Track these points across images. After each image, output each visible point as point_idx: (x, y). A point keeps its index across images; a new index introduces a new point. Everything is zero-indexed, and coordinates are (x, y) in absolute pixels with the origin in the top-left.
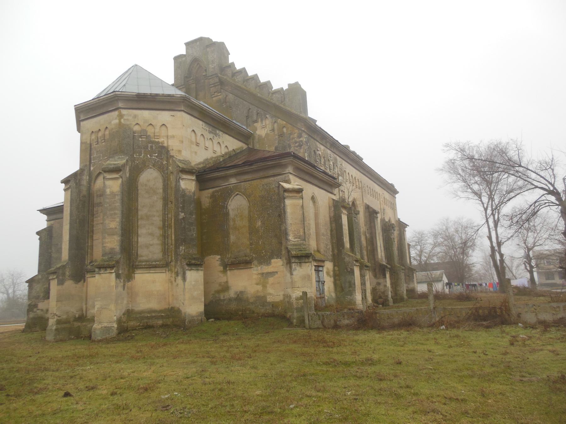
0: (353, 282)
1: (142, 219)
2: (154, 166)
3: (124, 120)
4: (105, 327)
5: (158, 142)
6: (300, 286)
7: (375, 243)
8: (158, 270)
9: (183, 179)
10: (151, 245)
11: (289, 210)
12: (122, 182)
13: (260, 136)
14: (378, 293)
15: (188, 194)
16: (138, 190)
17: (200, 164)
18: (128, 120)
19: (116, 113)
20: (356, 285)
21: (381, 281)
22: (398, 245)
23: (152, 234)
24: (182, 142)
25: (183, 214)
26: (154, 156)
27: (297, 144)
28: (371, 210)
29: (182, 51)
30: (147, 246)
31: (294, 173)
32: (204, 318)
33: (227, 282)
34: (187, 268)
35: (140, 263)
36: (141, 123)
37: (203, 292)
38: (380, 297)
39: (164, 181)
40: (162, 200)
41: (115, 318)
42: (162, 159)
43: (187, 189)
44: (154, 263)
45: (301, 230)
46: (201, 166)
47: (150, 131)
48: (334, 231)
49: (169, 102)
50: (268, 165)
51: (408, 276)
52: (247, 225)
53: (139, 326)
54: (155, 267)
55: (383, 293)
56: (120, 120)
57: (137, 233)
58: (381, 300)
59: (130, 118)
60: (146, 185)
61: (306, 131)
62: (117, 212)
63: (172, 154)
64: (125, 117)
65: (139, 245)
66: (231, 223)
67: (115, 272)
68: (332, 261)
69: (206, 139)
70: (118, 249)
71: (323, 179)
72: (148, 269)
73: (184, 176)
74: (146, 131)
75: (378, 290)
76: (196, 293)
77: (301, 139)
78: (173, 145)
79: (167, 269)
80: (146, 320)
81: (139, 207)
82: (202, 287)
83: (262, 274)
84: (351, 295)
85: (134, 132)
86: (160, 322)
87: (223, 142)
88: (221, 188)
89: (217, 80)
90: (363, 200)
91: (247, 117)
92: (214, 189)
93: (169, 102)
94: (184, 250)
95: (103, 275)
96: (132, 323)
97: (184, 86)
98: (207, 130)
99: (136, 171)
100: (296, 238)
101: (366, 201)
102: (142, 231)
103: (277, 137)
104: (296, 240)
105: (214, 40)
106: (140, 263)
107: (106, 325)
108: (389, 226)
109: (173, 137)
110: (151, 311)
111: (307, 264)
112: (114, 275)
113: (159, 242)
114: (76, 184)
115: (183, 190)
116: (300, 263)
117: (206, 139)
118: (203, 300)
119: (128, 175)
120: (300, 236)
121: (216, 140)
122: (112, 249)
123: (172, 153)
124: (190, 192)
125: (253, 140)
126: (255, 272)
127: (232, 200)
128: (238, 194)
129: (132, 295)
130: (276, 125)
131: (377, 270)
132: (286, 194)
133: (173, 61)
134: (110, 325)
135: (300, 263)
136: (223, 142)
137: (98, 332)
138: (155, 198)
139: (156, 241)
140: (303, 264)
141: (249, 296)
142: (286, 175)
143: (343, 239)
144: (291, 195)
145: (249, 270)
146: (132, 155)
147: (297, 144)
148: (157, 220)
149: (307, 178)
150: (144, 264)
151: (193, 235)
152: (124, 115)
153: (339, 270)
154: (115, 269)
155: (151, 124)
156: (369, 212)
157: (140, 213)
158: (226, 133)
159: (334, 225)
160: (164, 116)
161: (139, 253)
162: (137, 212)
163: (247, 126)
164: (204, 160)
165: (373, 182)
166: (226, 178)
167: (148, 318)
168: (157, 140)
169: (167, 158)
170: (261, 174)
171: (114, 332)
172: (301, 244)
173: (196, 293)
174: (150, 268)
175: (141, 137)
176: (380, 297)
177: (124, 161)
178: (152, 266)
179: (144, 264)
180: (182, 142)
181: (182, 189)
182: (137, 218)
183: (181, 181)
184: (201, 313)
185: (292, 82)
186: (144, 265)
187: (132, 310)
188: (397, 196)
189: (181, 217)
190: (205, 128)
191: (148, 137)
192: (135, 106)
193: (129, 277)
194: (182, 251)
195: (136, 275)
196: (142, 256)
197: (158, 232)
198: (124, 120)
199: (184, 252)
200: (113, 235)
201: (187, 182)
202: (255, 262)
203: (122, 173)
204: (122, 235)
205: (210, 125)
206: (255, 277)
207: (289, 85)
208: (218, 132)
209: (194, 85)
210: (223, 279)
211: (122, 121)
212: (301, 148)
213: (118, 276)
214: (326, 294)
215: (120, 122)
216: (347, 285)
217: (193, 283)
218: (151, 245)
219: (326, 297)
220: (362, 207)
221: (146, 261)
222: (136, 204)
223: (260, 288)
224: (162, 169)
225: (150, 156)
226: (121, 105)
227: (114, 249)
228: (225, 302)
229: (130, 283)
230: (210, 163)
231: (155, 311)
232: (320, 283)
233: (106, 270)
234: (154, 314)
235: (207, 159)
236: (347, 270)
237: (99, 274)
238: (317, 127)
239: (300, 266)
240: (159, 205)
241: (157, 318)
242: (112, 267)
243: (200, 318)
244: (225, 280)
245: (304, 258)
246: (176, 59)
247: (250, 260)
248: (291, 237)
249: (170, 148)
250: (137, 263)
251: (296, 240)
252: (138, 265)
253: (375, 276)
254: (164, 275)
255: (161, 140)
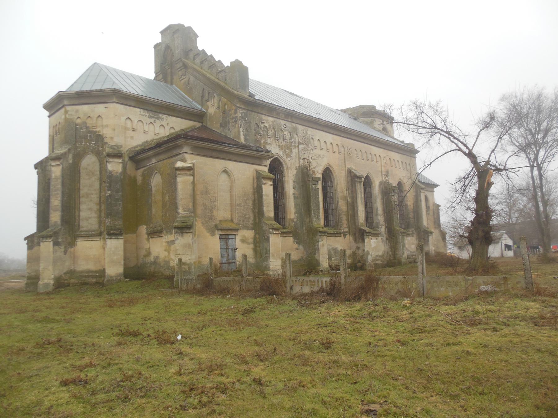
0: (268, 248)
1: (83, 196)
2: (92, 152)
3: (69, 115)
4: (46, 283)
5: (96, 132)
6: (181, 254)
7: (356, 208)
8: (94, 238)
9: (110, 162)
10: (90, 218)
11: (180, 186)
12: (63, 168)
13: (210, 114)
14: (358, 257)
15: (115, 174)
16: (80, 173)
17: (137, 146)
18: (71, 115)
19: (63, 110)
20: (271, 251)
21: (360, 245)
22: (414, 207)
23: (90, 209)
24: (114, 130)
25: (109, 192)
26: (93, 144)
27: (234, 120)
28: (352, 175)
29: (158, 39)
30: (87, 219)
31: (191, 152)
32: (122, 277)
33: (149, 248)
34: (107, 237)
35: (80, 233)
36: (81, 116)
37: (123, 257)
38: (359, 261)
39: (100, 164)
40: (98, 181)
41: (53, 277)
42: (98, 146)
43: (114, 171)
44: (91, 233)
45: (190, 203)
46: (139, 148)
47: (89, 122)
48: (257, 201)
49: (104, 96)
50: (170, 146)
51: (423, 239)
52: (161, 199)
53: (78, 283)
54: (92, 236)
55: (362, 257)
56: (65, 115)
57: (79, 209)
58: (360, 264)
59: (73, 113)
60: (86, 169)
61: (242, 106)
62: (58, 192)
63: (106, 141)
64: (69, 113)
65: (81, 218)
66: (153, 198)
67: (52, 241)
68: (252, 229)
69: (145, 124)
70: (59, 222)
71: (239, 153)
72: (87, 238)
73: (111, 160)
74: (86, 123)
75: (357, 255)
76: (115, 257)
77: (236, 115)
78: (107, 133)
79: (102, 238)
80: (84, 279)
81: (81, 187)
82: (122, 253)
83: (168, 242)
84: (267, 261)
85: (76, 125)
86: (94, 280)
87: (168, 124)
88: (147, 167)
89: (181, 64)
90: (345, 164)
91: (203, 97)
92: (145, 168)
93: (104, 96)
94: (110, 222)
95: (45, 243)
96: (72, 281)
97: (161, 72)
98: (146, 116)
99: (78, 157)
100: (185, 211)
101: (349, 165)
102: (83, 207)
103: (221, 114)
104: (185, 212)
105: (186, 26)
106: (80, 233)
107: (46, 281)
108: (389, 188)
109: (107, 126)
110: (89, 271)
111: (189, 234)
112: (52, 243)
113: (96, 215)
114: (42, 170)
115: (111, 172)
116: (182, 233)
117: (145, 124)
118: (123, 263)
119: (71, 161)
120: (189, 209)
121: (158, 123)
122: (56, 222)
123: (106, 140)
124: (117, 173)
125: (206, 118)
126: (164, 240)
127: (153, 178)
128: (156, 173)
129: (74, 258)
130: (220, 103)
131: (357, 235)
132: (178, 172)
133: (153, 50)
134: (49, 282)
135: (182, 233)
136: (168, 124)
137: (41, 287)
138: (93, 179)
139: (94, 215)
140: (185, 235)
141: (161, 260)
142: (182, 155)
143: (263, 208)
144: (182, 173)
145: (161, 238)
146: (75, 145)
147: (234, 120)
148: (95, 197)
149: (214, 154)
150: (83, 233)
151: (119, 209)
152: (68, 110)
153: (259, 238)
154: (52, 238)
155: (89, 117)
156: (351, 177)
157: (82, 192)
158: (172, 116)
159: (256, 195)
160: (100, 109)
161: (80, 225)
162: (79, 192)
163: (202, 105)
164: (142, 143)
165: (368, 145)
166: (149, 158)
167: (86, 277)
168: (94, 130)
169: (102, 144)
170: (169, 154)
171: (51, 288)
172: (190, 216)
173: (115, 257)
174: (88, 236)
175: (81, 128)
176: (359, 261)
177: (66, 150)
178: (89, 235)
179: (83, 233)
180: (114, 130)
181: (109, 171)
182: (79, 196)
183: (108, 164)
184: (120, 274)
185: (233, 60)
186: (83, 235)
187: (75, 271)
188: (417, 155)
189: (107, 195)
190: (144, 114)
191: (87, 127)
192: (77, 102)
193: (72, 244)
194: (107, 223)
195: (78, 243)
196: (83, 227)
197: (95, 207)
198: (69, 115)
199: (110, 223)
200: (57, 211)
201: (114, 164)
202: (164, 232)
203: (62, 160)
204: (63, 211)
205: (151, 111)
206: (164, 244)
207: (231, 63)
208: (160, 115)
209: (169, 70)
210: (147, 246)
211: (67, 116)
212: (236, 124)
213: (56, 244)
214: (237, 259)
215: (65, 117)
216: (264, 251)
217: (113, 249)
218: (90, 218)
219: (237, 263)
220: (344, 172)
221: (86, 231)
222: (78, 185)
223: (166, 253)
224: (98, 154)
225: (89, 144)
226: (66, 102)
227: (57, 222)
228: (149, 265)
229: (72, 249)
230: (151, 144)
231: (92, 272)
232: (230, 250)
233: (47, 239)
234: (90, 274)
235: (147, 142)
236: (265, 237)
237: (43, 242)
238: (257, 101)
239: (182, 236)
240: (97, 185)
241: (93, 277)
242: (50, 237)
243: (119, 278)
244: (149, 247)
245: (185, 229)
246: (198, 37)
247: (161, 229)
248: (180, 211)
249: (104, 136)
250: (78, 233)
251: (185, 212)
252: (78, 235)
253: (355, 240)
254: (99, 242)
255: (97, 130)
